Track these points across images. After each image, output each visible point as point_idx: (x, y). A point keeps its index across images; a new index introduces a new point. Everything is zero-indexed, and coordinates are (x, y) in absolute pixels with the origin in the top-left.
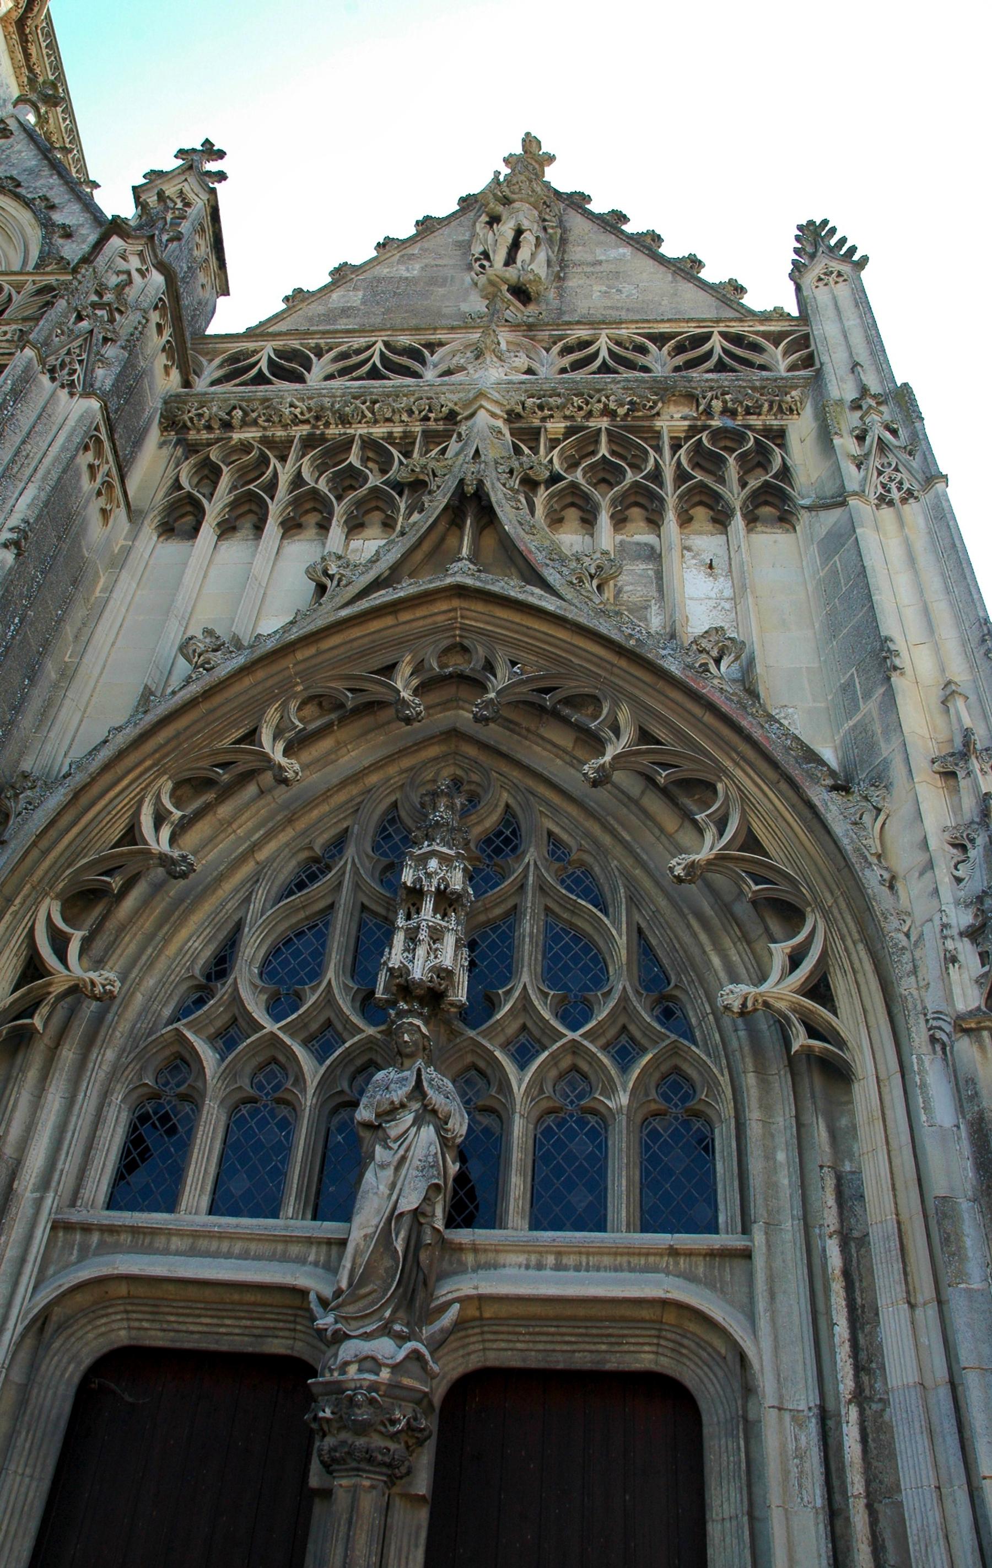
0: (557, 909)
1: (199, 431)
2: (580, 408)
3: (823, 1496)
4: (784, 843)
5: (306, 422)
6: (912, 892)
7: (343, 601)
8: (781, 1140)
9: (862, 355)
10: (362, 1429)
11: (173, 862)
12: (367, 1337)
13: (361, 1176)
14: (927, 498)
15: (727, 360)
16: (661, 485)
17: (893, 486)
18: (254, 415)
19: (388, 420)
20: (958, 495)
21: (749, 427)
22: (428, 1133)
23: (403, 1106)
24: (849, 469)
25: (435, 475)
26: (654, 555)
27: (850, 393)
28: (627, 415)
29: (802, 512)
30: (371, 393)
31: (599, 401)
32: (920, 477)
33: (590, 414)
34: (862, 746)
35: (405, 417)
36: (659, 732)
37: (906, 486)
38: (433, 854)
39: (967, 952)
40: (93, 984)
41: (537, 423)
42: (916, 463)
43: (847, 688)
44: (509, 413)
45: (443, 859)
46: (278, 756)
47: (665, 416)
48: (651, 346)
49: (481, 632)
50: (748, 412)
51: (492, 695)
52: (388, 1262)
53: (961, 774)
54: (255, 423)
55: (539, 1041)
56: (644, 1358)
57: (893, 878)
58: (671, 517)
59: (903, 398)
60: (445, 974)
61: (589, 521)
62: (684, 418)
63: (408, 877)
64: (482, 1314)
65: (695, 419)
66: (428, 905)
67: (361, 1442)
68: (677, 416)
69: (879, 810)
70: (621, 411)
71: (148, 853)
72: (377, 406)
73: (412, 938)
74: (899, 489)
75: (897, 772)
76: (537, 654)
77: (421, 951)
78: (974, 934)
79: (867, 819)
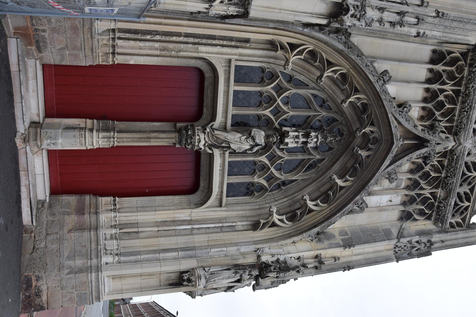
0: (304, 162)
1: (471, 56)
2: (450, 170)
3: (223, 104)
4: (307, 219)
5: (465, 91)
6: (291, 248)
7: (395, 115)
8: (244, 212)
9: (446, 243)
10: (186, 140)
11: (321, 79)
12: (205, 139)
13: (239, 132)
14: (393, 257)
15: (459, 207)
16: (419, 189)
17: (400, 249)
18: (472, 75)
19: (460, 116)
20: (393, 264)
21: (433, 212)
22: (248, 147)
23: (254, 141)
24: (408, 239)
25: (433, 133)
26: (397, 188)
27: (433, 240)
28: (445, 182)
29: (401, 224)
30: (470, 111)
31: (451, 175)
32: (400, 256)
33: (447, 171)
34: (330, 237)
35: (459, 121)
36: (342, 192)
37: (399, 252)
38: (318, 140)
39: (274, 259)
40: (288, 65)
41: (448, 157)
42: (405, 255)
43: (346, 234)
44: (453, 150)
45: (316, 142)
46: (352, 99)
47: (442, 191)
48: (470, 187)
49: (379, 148)
50: (438, 212)
51: (359, 152)
52: (220, 142)
53: (316, 260)
54: (469, 74)
55: (271, 160)
56: (202, 184)
57: (295, 243)
58: (407, 192)
59: (428, 253)
60: (287, 144)
61: (411, 171)
62: (440, 196)
63: (313, 134)
64: (211, 156)
65: (439, 198)
66: (304, 140)
67: (184, 140)
68: (441, 194)
69: (312, 240)
70: (446, 180)
71: (324, 71)
72: (465, 113)
73: (297, 137)
74: (399, 250)
75: (320, 245)
76: (370, 162)
77: (292, 140)
78: (278, 260)
79: (310, 238)
